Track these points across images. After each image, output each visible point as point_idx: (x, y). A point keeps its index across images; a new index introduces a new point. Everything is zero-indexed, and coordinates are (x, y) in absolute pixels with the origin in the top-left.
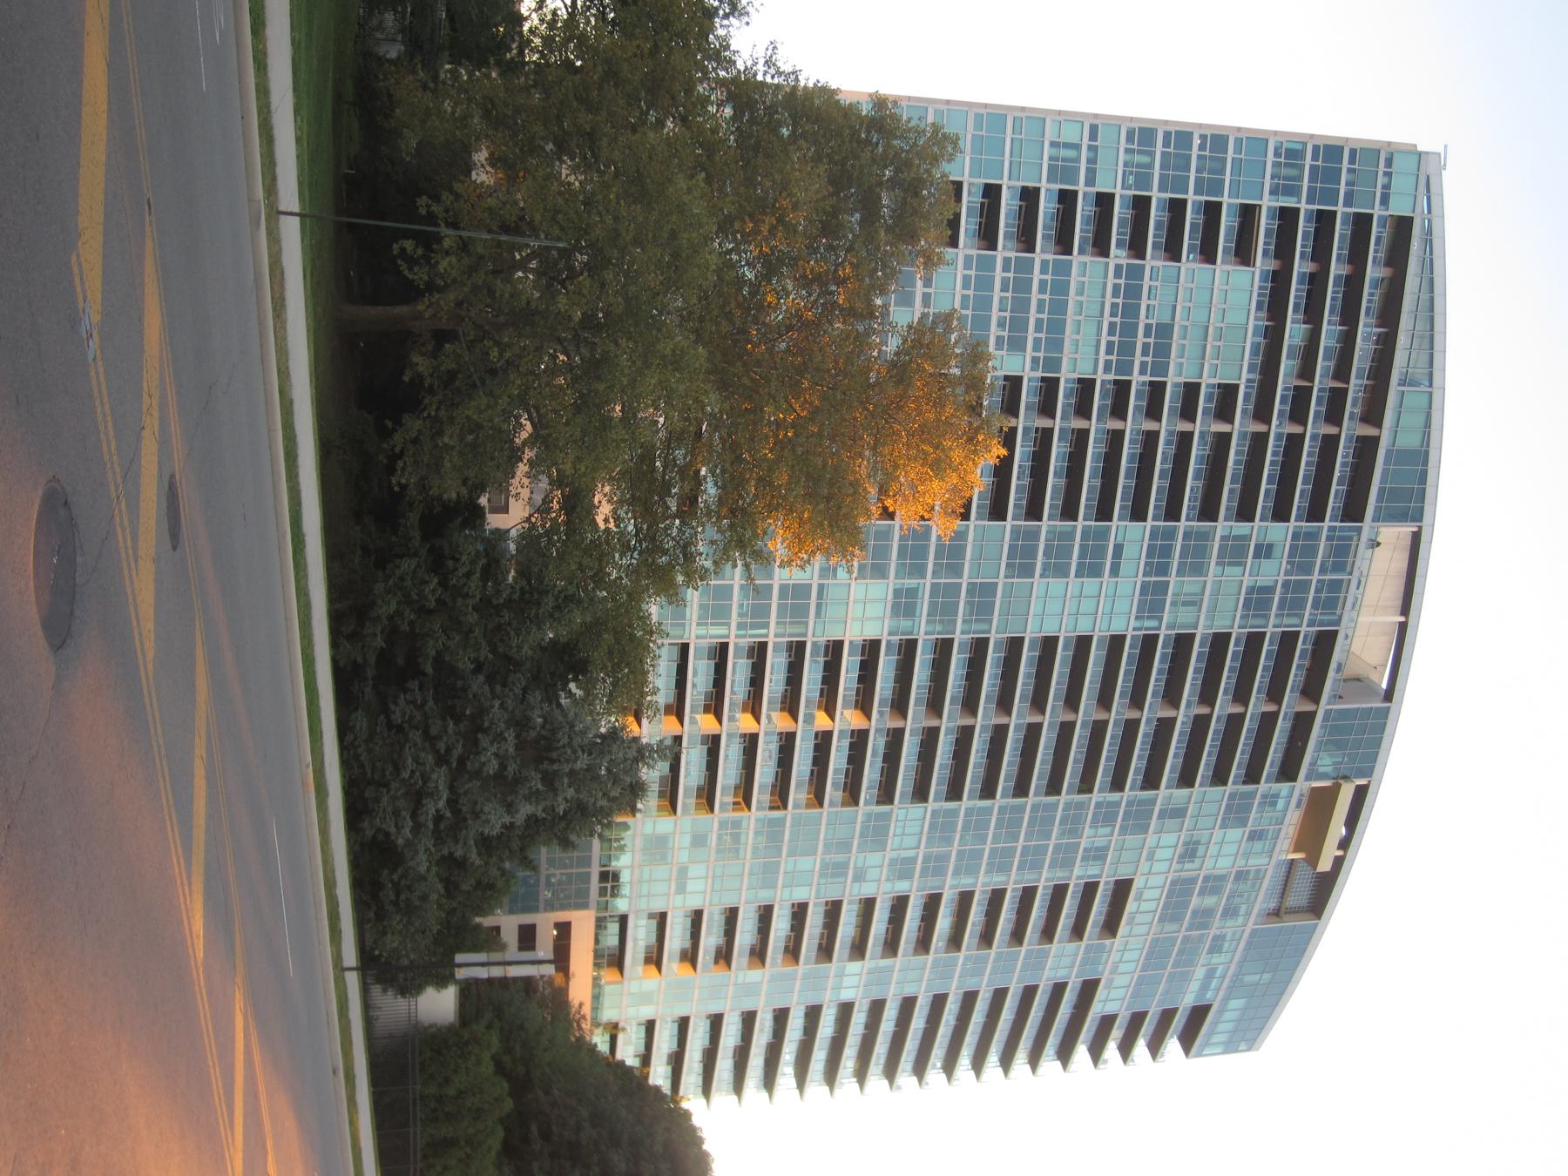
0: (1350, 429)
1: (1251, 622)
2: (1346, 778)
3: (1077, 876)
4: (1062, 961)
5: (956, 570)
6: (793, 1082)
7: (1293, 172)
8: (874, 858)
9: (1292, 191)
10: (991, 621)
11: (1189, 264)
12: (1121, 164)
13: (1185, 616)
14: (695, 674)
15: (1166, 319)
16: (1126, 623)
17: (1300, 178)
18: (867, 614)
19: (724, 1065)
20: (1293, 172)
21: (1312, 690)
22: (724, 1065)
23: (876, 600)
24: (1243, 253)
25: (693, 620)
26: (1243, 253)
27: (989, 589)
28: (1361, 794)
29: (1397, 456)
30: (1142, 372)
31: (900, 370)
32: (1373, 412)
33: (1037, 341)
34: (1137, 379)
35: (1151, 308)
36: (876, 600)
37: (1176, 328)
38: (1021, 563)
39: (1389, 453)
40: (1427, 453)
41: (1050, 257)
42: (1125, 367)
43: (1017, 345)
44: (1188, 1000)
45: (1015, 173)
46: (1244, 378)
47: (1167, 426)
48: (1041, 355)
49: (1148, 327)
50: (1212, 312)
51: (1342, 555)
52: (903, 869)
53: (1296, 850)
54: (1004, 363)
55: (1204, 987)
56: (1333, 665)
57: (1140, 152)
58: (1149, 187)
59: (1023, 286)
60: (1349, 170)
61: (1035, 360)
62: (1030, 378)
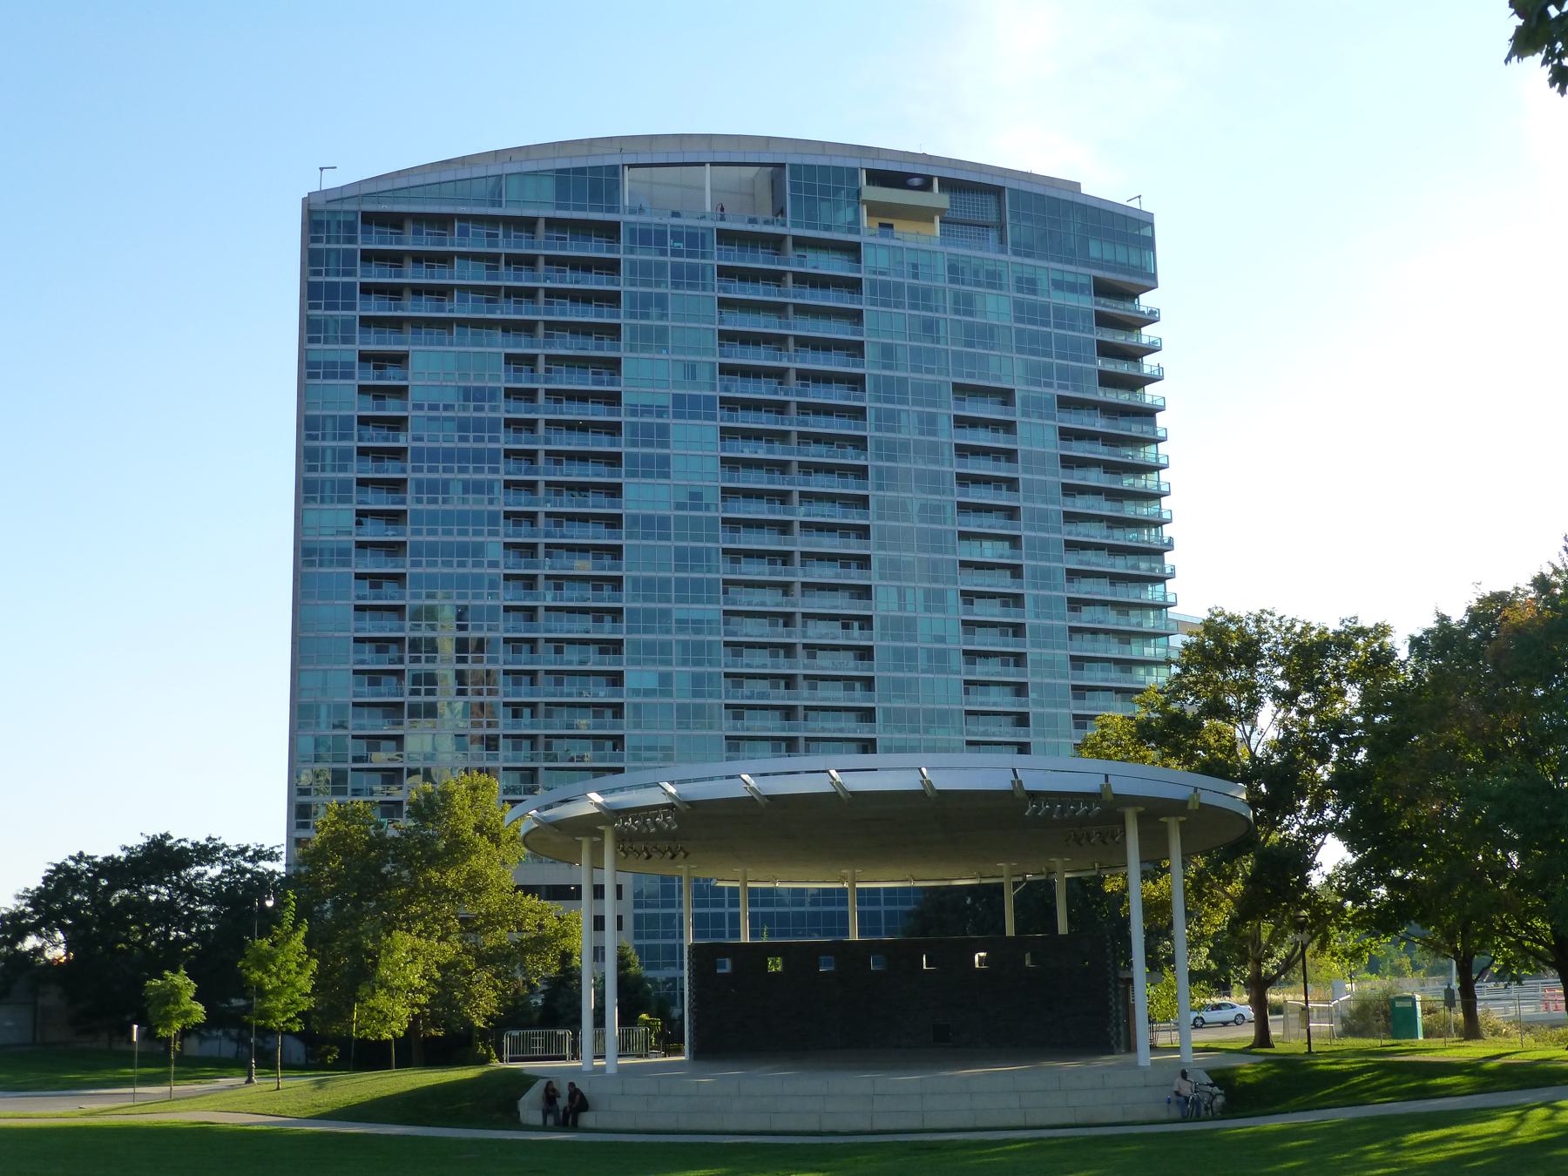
0: (542, 246)
1: (709, 281)
2: (859, 192)
3: (949, 436)
4: (1037, 437)
6: (1151, 449)
7: (329, 423)
13: (704, 375)
14: (763, 604)
15: (454, 425)
16: (710, 430)
19: (1129, 537)
20: (329, 423)
21: (774, 243)
22: (1129, 537)
24: (400, 359)
26: (400, 359)
27: (681, 554)
28: (880, 178)
29: (562, 198)
30: (496, 440)
32: (528, 224)
33: (476, 533)
38: (661, 467)
39: (559, 207)
40: (559, 171)
41: (408, 560)
42: (494, 423)
43: (478, 550)
44: (1088, 303)
46: (500, 346)
47: (543, 505)
48: (486, 529)
49: (462, 439)
51: (648, 237)
53: (932, 221)
55: (1073, 288)
56: (750, 228)
57: (323, 459)
58: (349, 450)
59: (432, 550)
60: (328, 242)
61: (491, 533)
62: (508, 533)
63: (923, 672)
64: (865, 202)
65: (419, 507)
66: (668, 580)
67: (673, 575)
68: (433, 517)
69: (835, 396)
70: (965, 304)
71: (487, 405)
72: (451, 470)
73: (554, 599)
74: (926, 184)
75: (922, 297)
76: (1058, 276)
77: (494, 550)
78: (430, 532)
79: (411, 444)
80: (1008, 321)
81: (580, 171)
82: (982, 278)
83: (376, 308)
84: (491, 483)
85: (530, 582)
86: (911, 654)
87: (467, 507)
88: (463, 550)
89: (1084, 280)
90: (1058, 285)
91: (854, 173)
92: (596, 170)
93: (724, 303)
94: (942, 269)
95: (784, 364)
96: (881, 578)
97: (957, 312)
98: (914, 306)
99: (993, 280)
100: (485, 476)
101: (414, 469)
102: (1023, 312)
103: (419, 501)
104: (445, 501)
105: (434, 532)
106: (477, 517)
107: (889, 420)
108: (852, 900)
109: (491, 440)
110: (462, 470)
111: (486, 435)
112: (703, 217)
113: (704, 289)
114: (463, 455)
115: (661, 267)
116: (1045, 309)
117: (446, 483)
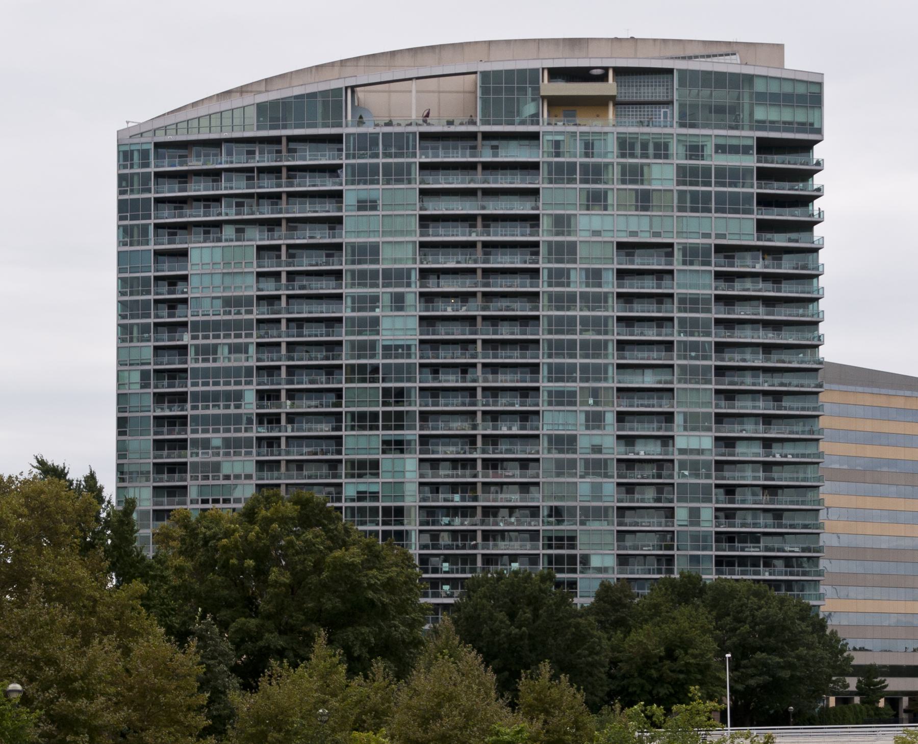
5: (375, 415)
8: (583, 443)
9: (145, 228)
10: (703, 342)
11: (191, 291)
12: (551, 186)
15: (219, 303)
17: (138, 225)
18: (390, 469)
23: (393, 464)
24: (184, 253)
25: (593, 600)
26: (184, 253)
27: (387, 392)
30: (251, 312)
31: (8, 482)
33: (236, 383)
34: (256, 315)
35: (213, 313)
36: (393, 464)
37: (225, 294)
45: (147, 409)
46: (257, 238)
49: (225, 313)
50: (217, 270)
52: (595, 420)
54: (250, 405)
55: (734, 150)
63: (581, 477)
64: (543, 97)
65: (196, 365)
66: (377, 413)
67: (380, 409)
68: (206, 373)
69: (515, 261)
70: (633, 174)
71: (243, 310)
72: (218, 337)
73: (293, 431)
74: (603, 78)
75: (595, 172)
76: (721, 141)
77: (250, 397)
78: (204, 384)
79: (190, 319)
80: (673, 186)
81: (313, 95)
82: (651, 151)
83: (171, 191)
84: (247, 345)
85: (273, 420)
86: (572, 463)
87: (230, 364)
88: (228, 396)
89: (749, 142)
90: (721, 149)
91: (534, 74)
92: (324, 93)
93: (424, 193)
94: (612, 145)
95: (473, 238)
96: (550, 404)
97: (623, 182)
98: (584, 181)
99: (661, 150)
100: (243, 340)
101: (193, 385)
102: (685, 175)
103: (197, 361)
104: (215, 360)
105: (207, 384)
106: (237, 371)
107: (560, 277)
108: (651, 155)
109: (247, 336)
110: (227, 336)
111: (243, 380)
112: (410, 124)
113: (410, 183)
114: (227, 325)
115: (374, 168)
116: (707, 171)
117: (215, 346)
